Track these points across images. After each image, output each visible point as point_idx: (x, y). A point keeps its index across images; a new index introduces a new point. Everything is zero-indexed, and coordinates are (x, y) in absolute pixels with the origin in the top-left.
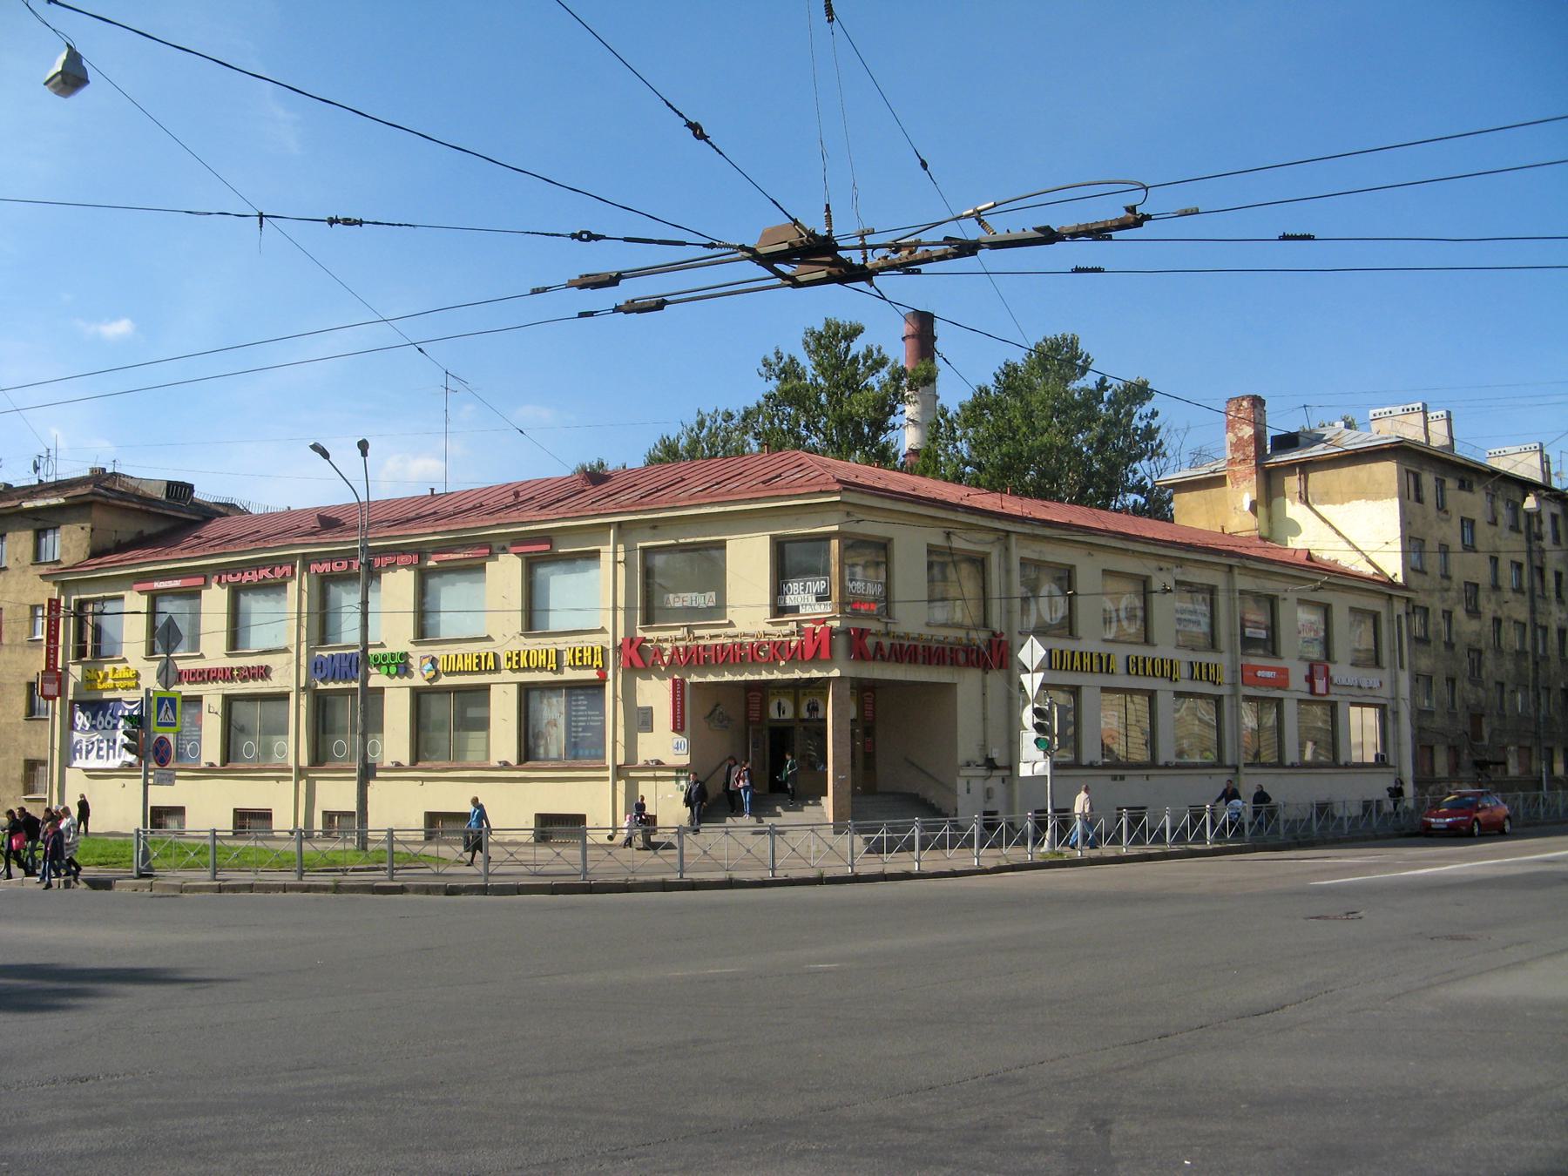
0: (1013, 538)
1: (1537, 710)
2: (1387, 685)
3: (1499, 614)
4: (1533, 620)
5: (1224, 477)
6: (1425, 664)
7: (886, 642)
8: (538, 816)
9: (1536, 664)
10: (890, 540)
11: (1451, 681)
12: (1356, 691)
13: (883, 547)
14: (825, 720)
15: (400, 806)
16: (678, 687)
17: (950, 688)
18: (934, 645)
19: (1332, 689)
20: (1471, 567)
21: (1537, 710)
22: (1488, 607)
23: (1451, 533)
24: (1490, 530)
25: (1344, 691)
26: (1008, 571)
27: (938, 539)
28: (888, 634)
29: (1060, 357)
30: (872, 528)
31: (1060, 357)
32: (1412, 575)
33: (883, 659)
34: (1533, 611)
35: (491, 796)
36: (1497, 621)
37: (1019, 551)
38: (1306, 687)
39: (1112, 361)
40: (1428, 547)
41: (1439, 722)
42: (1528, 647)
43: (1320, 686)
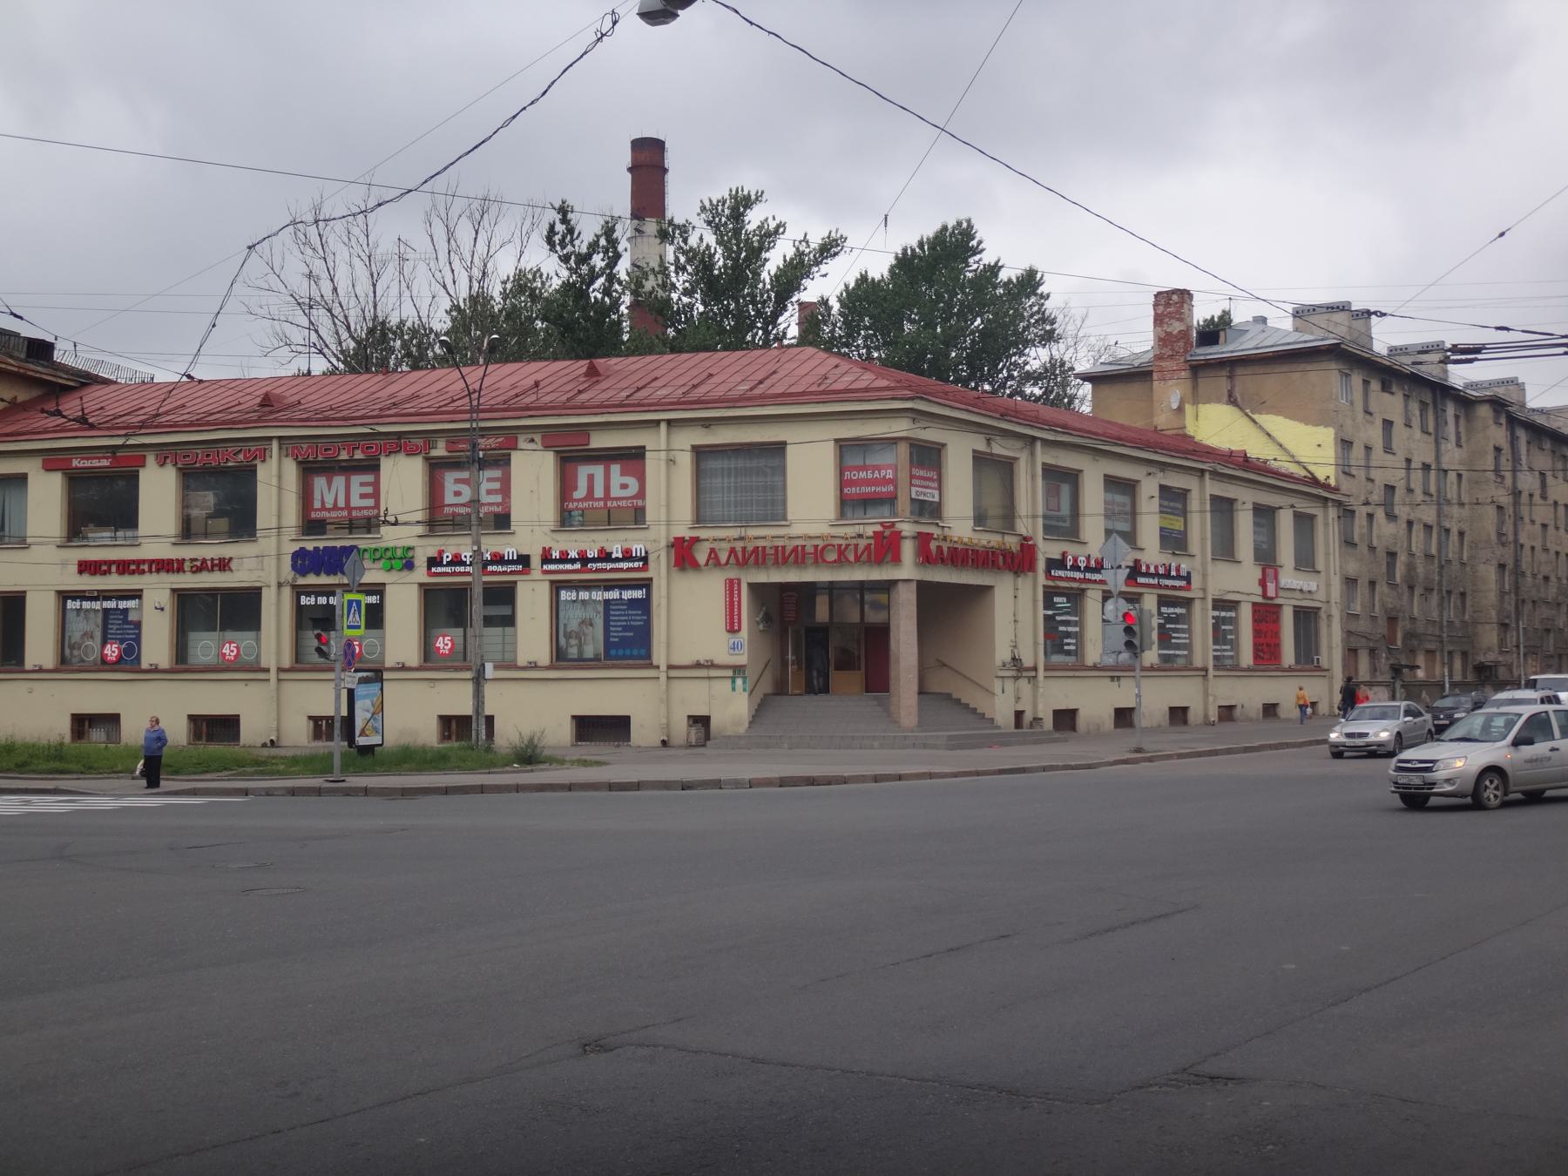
0: (1039, 444)
1: (1441, 615)
2: (1323, 588)
3: (1412, 517)
4: (1439, 524)
5: (1151, 373)
6: (1353, 568)
7: (945, 546)
8: (193, 718)
9: (1441, 567)
10: (944, 445)
11: (1372, 583)
12: (1298, 595)
13: (1183, 495)
14: (1560, 672)
15: (411, 712)
16: (732, 586)
17: (988, 589)
18: (960, 547)
19: (1281, 594)
20: (1389, 470)
21: (1441, 615)
22: (1401, 511)
23: (1375, 434)
24: (1405, 432)
25: (1289, 594)
26: (1033, 477)
27: (981, 446)
28: (945, 539)
29: (953, 246)
30: (1000, 449)
31: (953, 246)
32: (1343, 477)
33: (943, 561)
34: (1439, 515)
35: (497, 700)
36: (1410, 523)
37: (1043, 456)
38: (1259, 590)
39: (1004, 249)
40: (1413, 465)
41: (1363, 626)
42: (1434, 551)
43: (1271, 588)
